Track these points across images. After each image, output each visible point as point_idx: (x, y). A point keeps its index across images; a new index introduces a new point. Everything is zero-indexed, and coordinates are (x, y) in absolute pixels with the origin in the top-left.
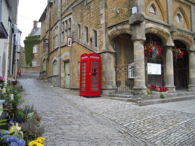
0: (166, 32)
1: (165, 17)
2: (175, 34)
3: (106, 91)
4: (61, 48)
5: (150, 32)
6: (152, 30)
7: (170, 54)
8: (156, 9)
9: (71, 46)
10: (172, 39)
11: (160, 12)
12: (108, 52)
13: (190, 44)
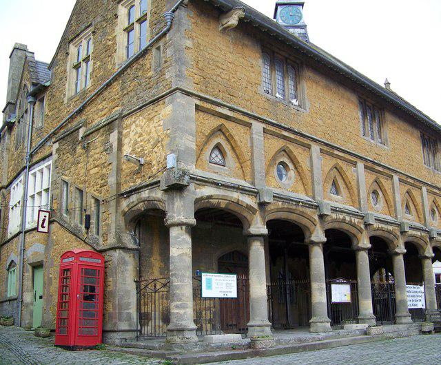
1: (248, 171)
2: (269, 208)
3: (115, 334)
4: (26, 232)
5: (208, 205)
6: (214, 201)
7: (258, 252)
9: (46, 230)
10: (263, 218)
11: (237, 161)
12: (119, 248)
13: (312, 228)
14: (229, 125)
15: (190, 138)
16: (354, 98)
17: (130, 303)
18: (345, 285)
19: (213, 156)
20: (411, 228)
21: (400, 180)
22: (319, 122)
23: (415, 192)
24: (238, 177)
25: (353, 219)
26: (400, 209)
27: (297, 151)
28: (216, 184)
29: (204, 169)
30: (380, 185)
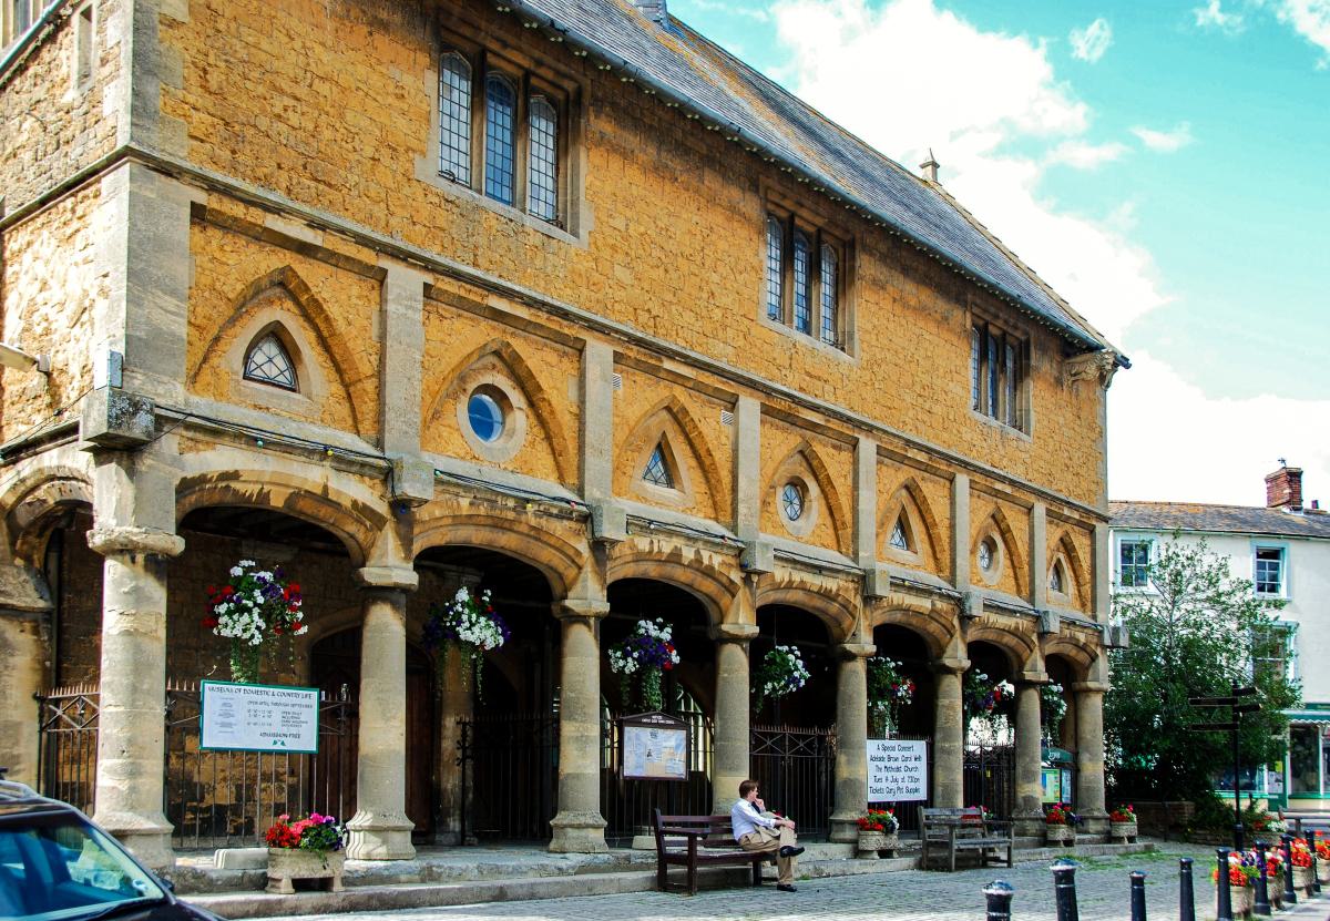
0: (355, 503)
1: (367, 408)
5: (229, 498)
7: (386, 632)
8: (301, 360)
10: (406, 541)
11: (334, 376)
14: (306, 270)
15: (171, 303)
16: (751, 206)
17: (18, 756)
18: (669, 732)
19: (259, 358)
20: (987, 607)
21: (1049, 513)
22: (621, 273)
23: (933, 491)
24: (335, 422)
25: (705, 555)
26: (1044, 578)
27: (540, 360)
28: (249, 438)
29: (220, 395)
30: (815, 463)
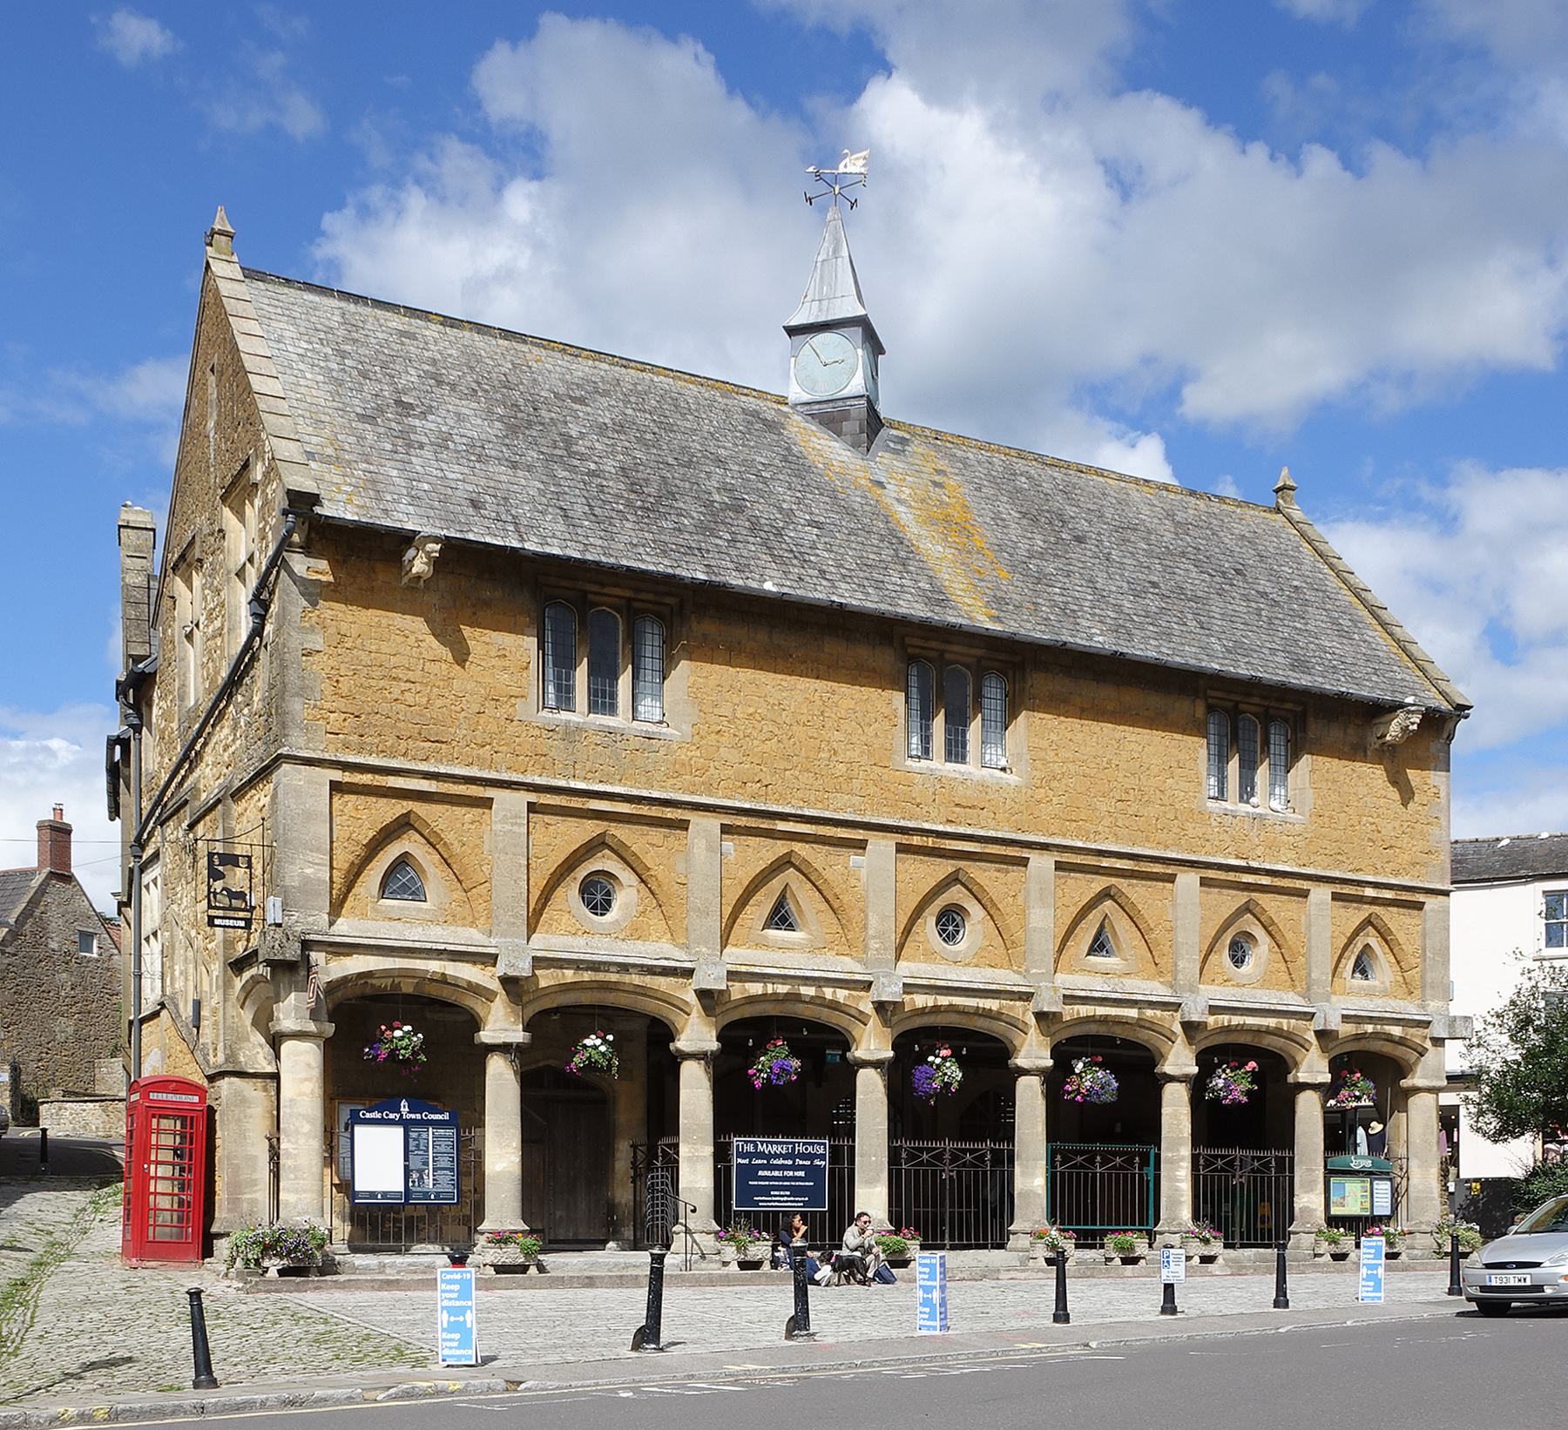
5: (368, 991)
7: (501, 1079)
24: (1278, 985)
30: (975, 889)
